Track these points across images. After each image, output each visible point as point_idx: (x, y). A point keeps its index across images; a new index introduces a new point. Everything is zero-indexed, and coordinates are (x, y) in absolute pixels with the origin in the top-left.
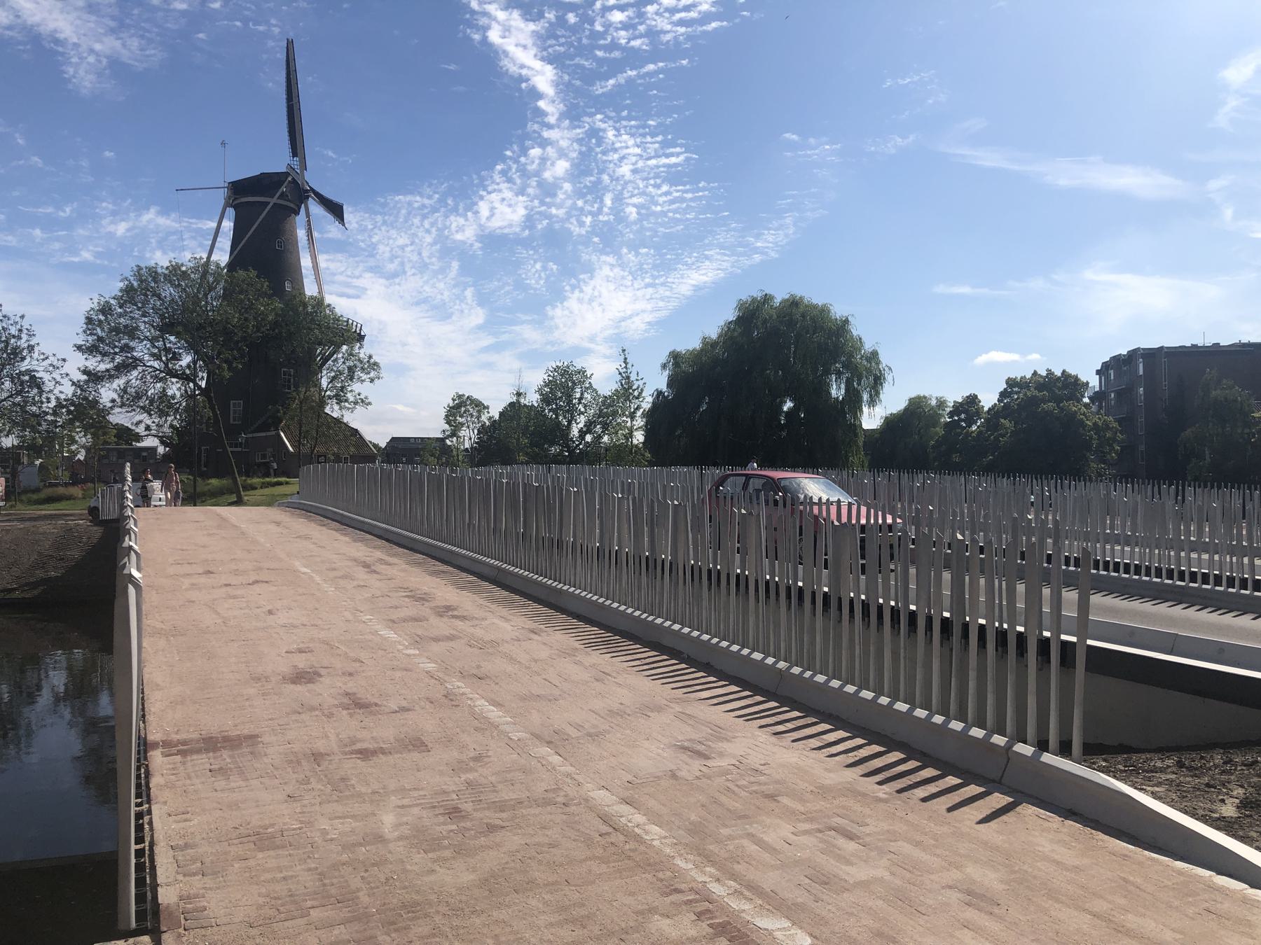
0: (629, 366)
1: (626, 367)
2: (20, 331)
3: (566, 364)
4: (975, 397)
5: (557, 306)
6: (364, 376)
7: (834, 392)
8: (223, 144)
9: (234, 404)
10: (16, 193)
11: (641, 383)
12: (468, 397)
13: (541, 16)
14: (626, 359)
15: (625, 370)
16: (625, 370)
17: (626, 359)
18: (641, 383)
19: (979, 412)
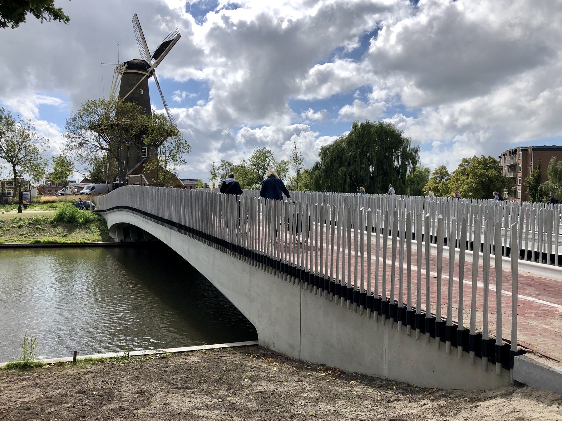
0: (297, 149)
1: (296, 150)
2: (29, 127)
3: (262, 148)
4: (445, 167)
5: (358, 95)
6: (184, 151)
7: (396, 163)
8: (118, 44)
9: (145, 156)
10: (510, 364)
11: (302, 157)
12: (227, 162)
13: (198, 94)
14: (295, 146)
15: (295, 151)
16: (295, 151)
17: (295, 146)
18: (302, 157)
19: (446, 174)
